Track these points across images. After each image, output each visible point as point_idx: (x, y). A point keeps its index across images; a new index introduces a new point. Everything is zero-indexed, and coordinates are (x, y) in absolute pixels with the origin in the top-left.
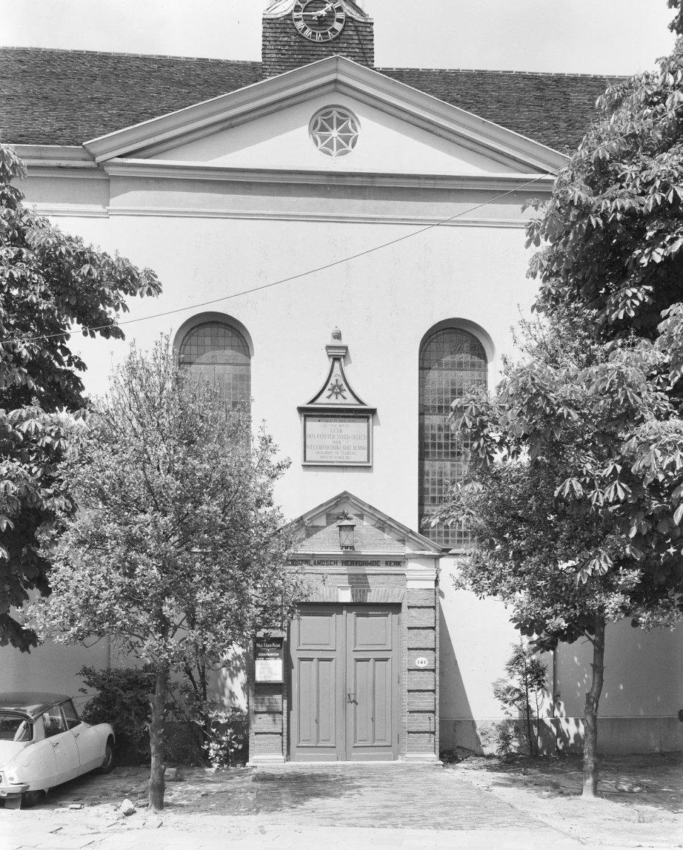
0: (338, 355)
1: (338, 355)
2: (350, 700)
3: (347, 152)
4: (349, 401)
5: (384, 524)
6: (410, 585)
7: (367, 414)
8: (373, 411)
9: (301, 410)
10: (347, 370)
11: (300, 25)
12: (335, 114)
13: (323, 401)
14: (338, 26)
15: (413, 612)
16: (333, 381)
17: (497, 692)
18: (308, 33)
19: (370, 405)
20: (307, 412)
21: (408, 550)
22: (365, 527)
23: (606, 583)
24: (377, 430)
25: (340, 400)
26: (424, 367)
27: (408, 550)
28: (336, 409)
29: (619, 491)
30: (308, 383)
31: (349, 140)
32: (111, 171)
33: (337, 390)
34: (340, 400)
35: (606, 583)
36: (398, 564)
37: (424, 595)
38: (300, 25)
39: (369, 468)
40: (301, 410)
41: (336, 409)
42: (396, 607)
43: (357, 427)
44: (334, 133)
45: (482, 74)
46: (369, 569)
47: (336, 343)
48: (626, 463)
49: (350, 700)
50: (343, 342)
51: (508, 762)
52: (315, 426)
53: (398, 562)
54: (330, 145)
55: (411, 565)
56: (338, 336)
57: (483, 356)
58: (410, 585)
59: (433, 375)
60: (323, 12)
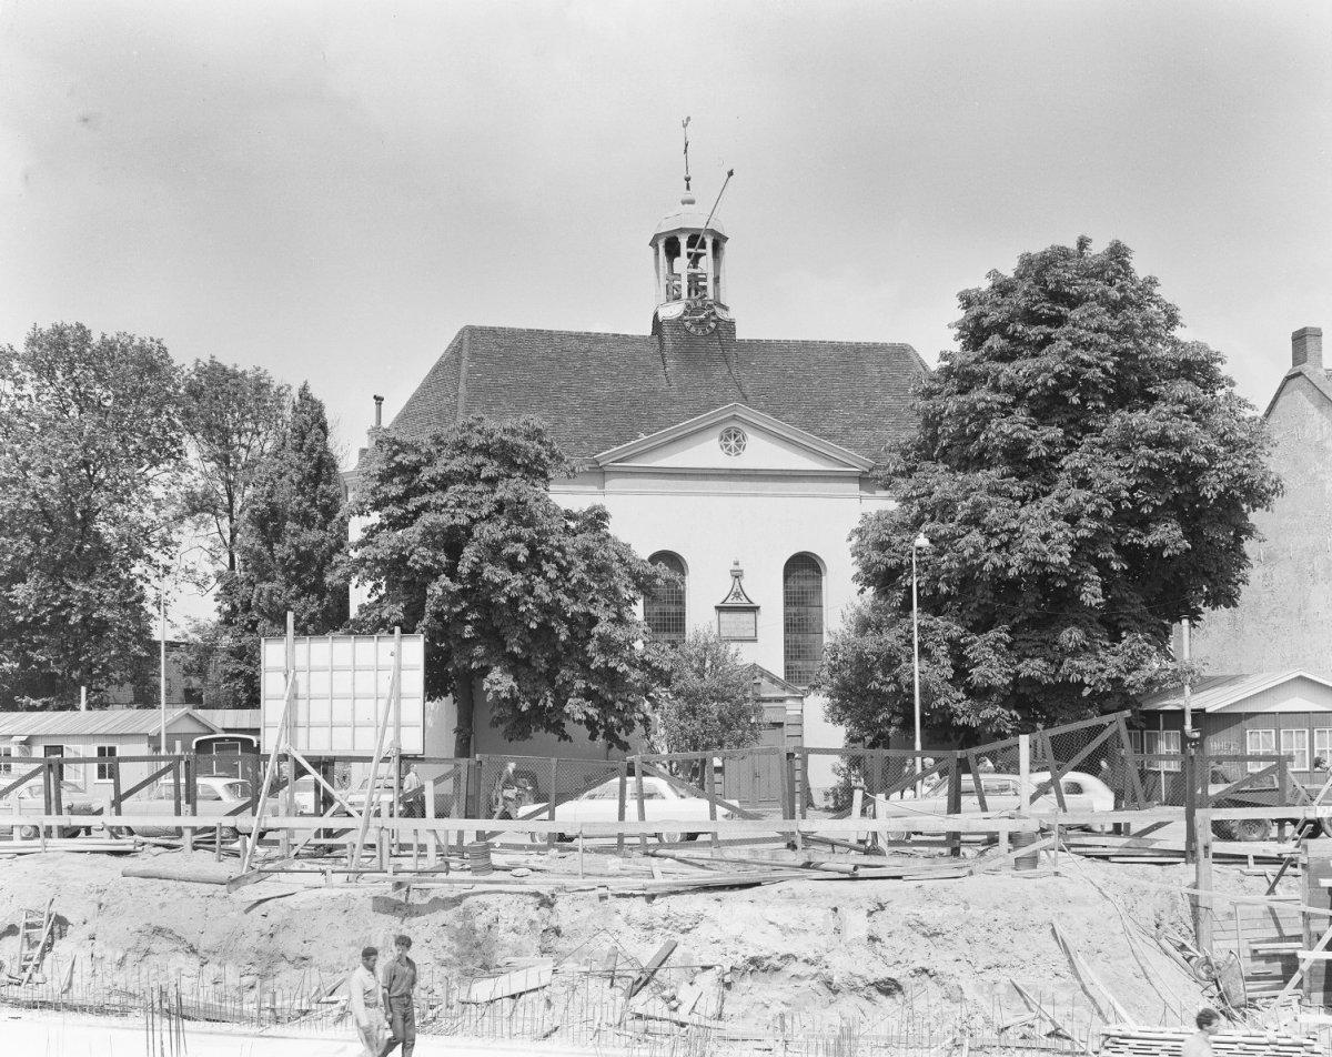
0: (737, 575)
1: (737, 575)
2: (756, 775)
3: (739, 454)
4: (743, 602)
5: (774, 680)
6: (788, 713)
7: (755, 609)
8: (758, 608)
9: (717, 608)
10: (742, 582)
11: (688, 324)
12: (733, 432)
13: (731, 602)
14: (713, 325)
15: (789, 727)
16: (734, 590)
17: (834, 770)
18: (693, 330)
19: (756, 605)
20: (720, 609)
21: (787, 694)
22: (764, 682)
23: (888, 723)
24: (759, 617)
25: (739, 601)
26: (786, 577)
27: (787, 694)
28: (738, 607)
29: (892, 688)
30: (721, 591)
31: (740, 446)
32: (606, 469)
33: (737, 595)
34: (739, 601)
35: (888, 723)
36: (781, 701)
37: (796, 718)
38: (688, 324)
39: (755, 641)
40: (717, 608)
41: (738, 607)
42: (780, 725)
43: (748, 617)
44: (732, 443)
45: (805, 343)
46: (764, 705)
47: (736, 568)
48: (896, 677)
49: (756, 775)
50: (740, 567)
51: (893, 723)
52: (725, 616)
53: (781, 700)
54: (730, 450)
55: (788, 702)
56: (737, 564)
57: (819, 571)
58: (788, 713)
59: (791, 584)
60: (702, 316)
